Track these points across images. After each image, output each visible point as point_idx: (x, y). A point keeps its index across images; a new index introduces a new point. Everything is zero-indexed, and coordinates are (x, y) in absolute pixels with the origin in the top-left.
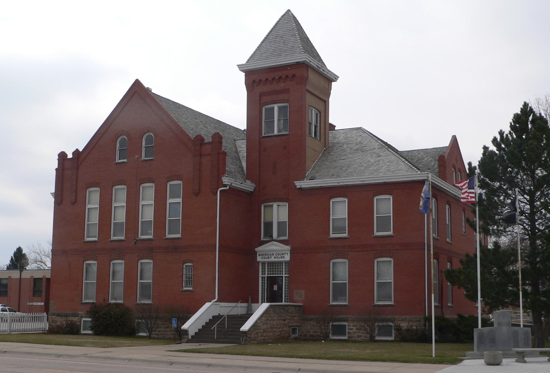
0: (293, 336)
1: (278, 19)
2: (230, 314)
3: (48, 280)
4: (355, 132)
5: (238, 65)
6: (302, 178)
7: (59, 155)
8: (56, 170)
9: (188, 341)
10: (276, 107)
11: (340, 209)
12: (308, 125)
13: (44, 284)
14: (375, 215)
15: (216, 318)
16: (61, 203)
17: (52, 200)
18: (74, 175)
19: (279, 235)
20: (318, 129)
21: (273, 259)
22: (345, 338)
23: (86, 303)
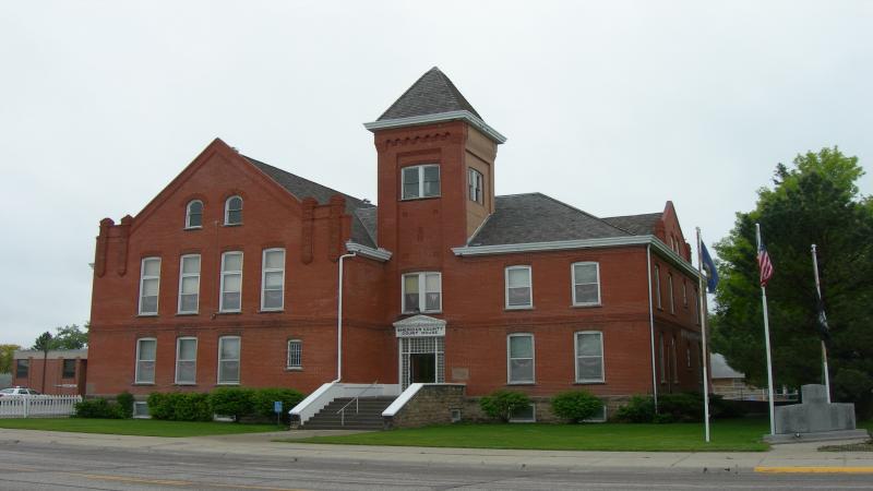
0: (454, 420)
1: (420, 77)
2: (364, 395)
3: (84, 362)
4: (445, 83)
5: (365, 124)
6: (462, 243)
7: (101, 222)
8: (98, 238)
9: (301, 428)
10: (421, 169)
11: (520, 280)
12: (467, 187)
13: (78, 365)
14: (574, 284)
15: (338, 402)
16: (103, 275)
17: (91, 272)
18: (118, 246)
19: (428, 308)
20: (480, 193)
21: (419, 334)
22: (534, 421)
23: (139, 385)
